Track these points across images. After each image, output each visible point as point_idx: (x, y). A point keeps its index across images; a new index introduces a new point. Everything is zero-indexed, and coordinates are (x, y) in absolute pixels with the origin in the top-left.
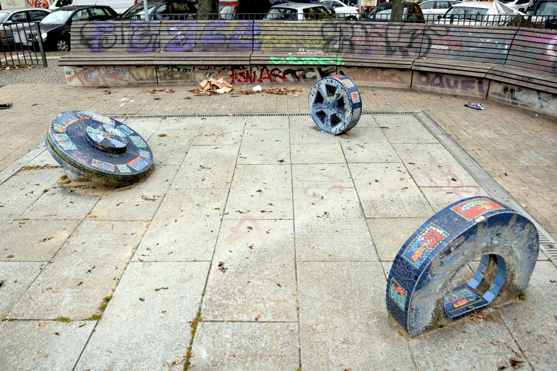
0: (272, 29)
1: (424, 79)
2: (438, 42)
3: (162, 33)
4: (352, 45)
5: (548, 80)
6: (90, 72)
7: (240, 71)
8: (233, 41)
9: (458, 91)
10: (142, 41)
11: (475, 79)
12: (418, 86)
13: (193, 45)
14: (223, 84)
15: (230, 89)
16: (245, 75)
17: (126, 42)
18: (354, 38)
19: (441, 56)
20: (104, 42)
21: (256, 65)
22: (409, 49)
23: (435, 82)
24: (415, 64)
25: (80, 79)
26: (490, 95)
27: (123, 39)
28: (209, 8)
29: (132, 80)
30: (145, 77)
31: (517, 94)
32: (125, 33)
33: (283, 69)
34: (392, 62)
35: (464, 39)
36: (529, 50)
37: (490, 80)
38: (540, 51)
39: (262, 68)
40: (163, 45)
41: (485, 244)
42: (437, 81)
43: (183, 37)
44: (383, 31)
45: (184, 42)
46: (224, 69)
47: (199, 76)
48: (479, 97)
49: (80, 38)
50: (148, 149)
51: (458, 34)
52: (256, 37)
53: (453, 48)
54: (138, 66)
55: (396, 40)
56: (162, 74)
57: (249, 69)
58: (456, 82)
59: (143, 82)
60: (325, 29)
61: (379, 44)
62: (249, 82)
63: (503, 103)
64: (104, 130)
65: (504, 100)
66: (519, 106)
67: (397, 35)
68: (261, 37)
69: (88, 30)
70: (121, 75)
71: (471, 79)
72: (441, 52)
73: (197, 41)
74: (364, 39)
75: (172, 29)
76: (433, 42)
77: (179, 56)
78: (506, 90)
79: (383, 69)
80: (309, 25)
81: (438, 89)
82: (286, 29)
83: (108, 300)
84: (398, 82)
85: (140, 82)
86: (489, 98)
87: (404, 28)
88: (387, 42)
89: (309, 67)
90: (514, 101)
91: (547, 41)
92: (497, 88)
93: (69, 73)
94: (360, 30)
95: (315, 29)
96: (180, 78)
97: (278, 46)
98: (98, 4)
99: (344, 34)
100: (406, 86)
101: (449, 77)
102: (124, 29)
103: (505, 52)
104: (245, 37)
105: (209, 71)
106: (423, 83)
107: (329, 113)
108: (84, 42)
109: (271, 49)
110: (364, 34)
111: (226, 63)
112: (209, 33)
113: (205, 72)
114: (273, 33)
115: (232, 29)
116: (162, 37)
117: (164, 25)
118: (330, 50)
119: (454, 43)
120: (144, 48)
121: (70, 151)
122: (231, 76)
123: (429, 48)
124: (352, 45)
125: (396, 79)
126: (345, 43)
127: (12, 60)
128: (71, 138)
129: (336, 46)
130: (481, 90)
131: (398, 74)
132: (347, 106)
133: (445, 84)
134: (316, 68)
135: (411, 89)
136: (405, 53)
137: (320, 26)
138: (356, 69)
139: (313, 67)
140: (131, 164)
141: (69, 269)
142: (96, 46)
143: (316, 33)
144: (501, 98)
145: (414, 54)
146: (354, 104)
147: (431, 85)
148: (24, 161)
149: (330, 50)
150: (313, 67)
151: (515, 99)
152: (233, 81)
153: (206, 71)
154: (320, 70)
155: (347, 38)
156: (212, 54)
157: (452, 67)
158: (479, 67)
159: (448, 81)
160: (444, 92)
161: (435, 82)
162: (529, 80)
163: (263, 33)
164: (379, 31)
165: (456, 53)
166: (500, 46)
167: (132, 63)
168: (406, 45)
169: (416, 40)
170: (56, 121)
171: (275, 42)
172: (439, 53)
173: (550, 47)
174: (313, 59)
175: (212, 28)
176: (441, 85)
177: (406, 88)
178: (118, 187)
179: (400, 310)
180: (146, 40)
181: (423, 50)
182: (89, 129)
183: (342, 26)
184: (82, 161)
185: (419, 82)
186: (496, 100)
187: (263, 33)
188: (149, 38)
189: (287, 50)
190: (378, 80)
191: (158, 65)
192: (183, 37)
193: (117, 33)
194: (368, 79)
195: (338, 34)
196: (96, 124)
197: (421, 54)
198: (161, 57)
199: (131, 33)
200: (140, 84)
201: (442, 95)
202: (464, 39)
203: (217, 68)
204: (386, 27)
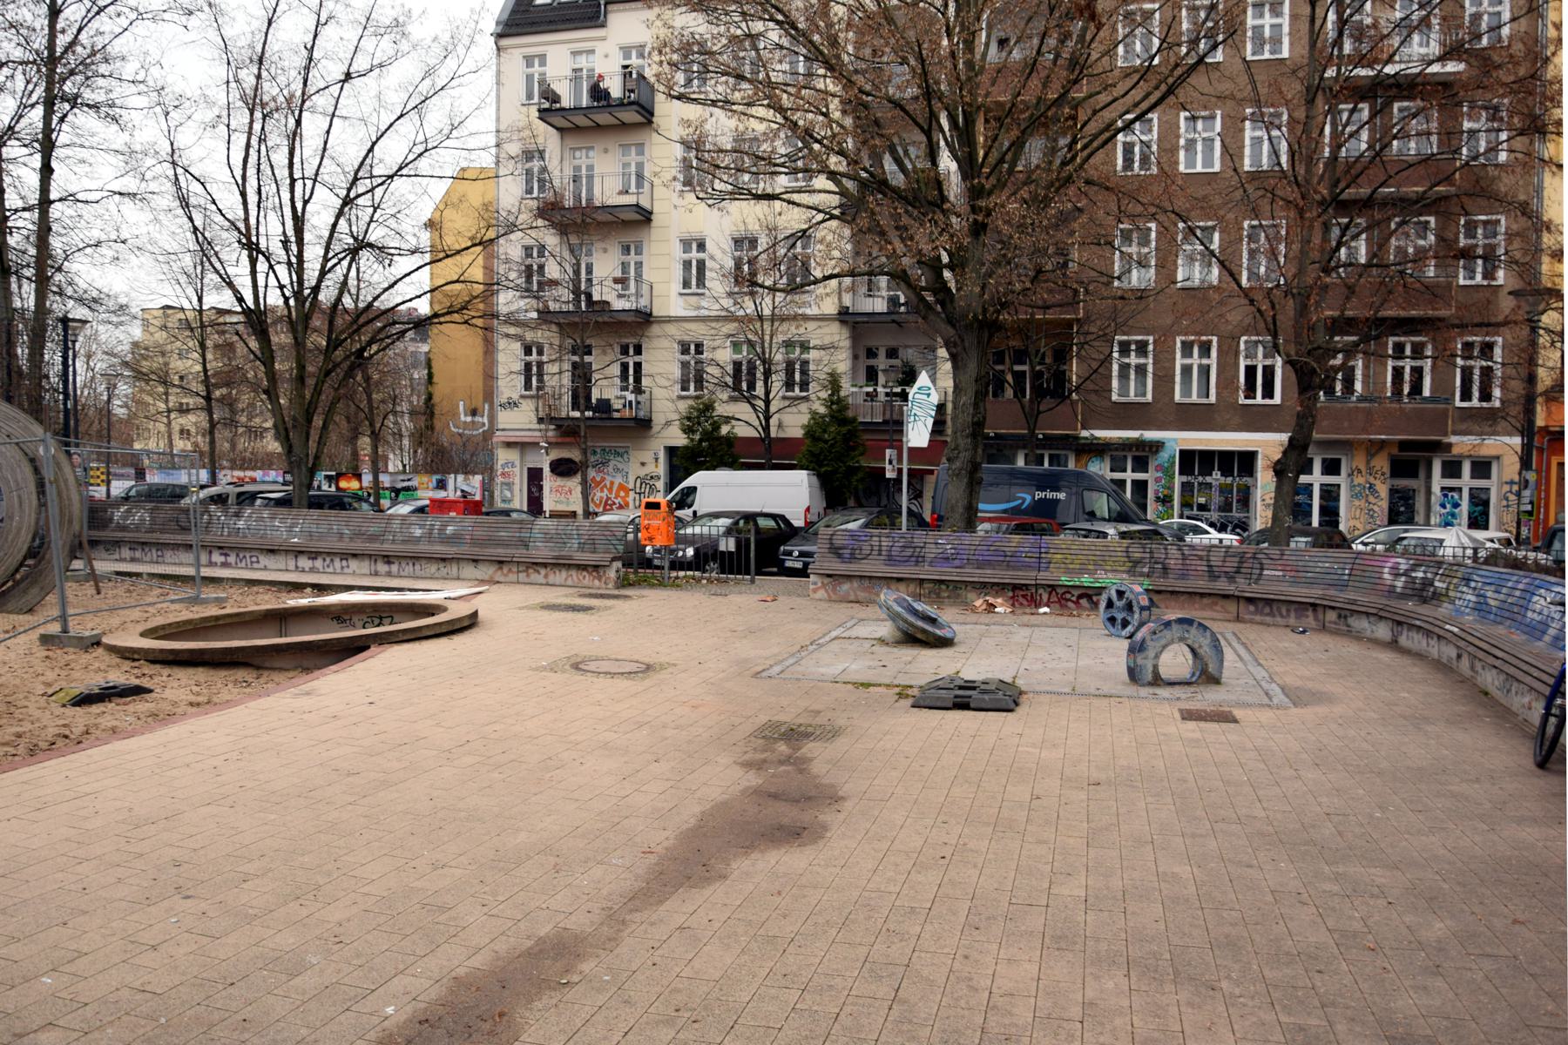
1: (1252, 608)
9: (1292, 621)
21: (1043, 586)
31: (1351, 621)
33: (1076, 593)
37: (1325, 606)
42: (1267, 610)
47: (971, 596)
77: (949, 573)
78: (1340, 616)
81: (1268, 619)
92: (1331, 616)
98: (766, 510)
107: (1119, 616)
129: (1146, 570)
130: (1316, 619)
131: (1222, 602)
132: (1136, 609)
135: (1238, 619)
136: (1231, 579)
162: (1354, 602)
172: (1272, 579)
176: (1271, 614)
180: (909, 552)
185: (1247, 611)
189: (1082, 571)
198: (926, 572)
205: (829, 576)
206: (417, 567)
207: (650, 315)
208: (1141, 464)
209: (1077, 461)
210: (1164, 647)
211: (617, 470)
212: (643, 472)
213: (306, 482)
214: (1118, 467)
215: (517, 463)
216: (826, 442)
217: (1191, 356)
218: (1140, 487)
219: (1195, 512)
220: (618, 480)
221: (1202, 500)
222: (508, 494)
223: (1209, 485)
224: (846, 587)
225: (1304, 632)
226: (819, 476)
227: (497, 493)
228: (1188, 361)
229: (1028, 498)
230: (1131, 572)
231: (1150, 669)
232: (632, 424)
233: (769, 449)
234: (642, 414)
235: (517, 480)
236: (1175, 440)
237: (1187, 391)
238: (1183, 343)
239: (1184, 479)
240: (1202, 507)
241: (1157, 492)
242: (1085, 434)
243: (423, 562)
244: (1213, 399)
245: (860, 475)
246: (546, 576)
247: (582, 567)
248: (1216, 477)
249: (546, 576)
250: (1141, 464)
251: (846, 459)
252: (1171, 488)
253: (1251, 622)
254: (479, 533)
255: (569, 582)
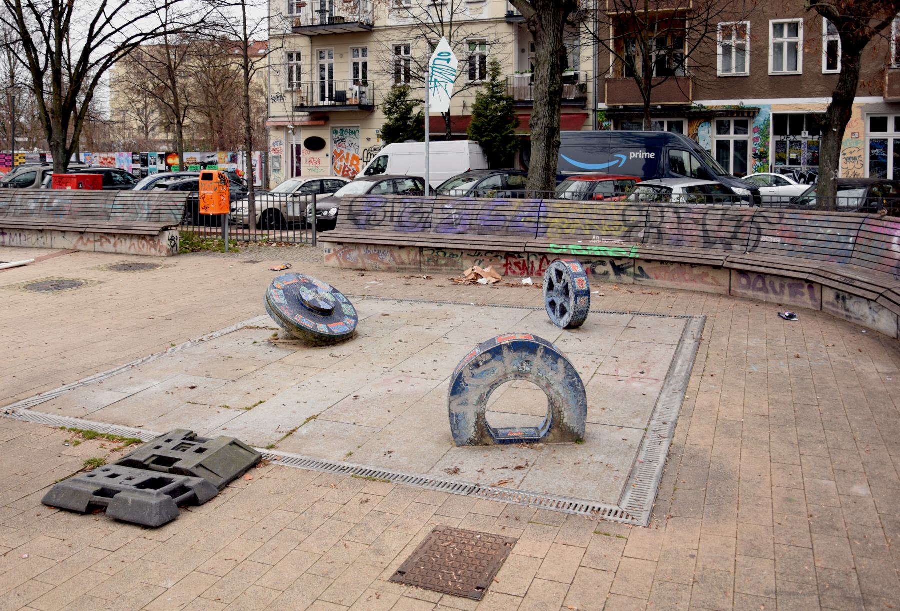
0: (562, 210)
1: (744, 281)
2: (770, 232)
3: (435, 211)
4: (660, 233)
5: (873, 282)
6: (350, 251)
7: (515, 260)
8: (514, 224)
10: (413, 220)
11: (804, 282)
12: (739, 291)
13: (468, 227)
14: (488, 273)
15: (495, 280)
16: (521, 266)
17: (395, 219)
18: (663, 225)
19: (773, 251)
20: (372, 218)
21: (534, 253)
22: (733, 241)
23: (758, 286)
24: (729, 259)
25: (338, 258)
26: (824, 305)
27: (392, 216)
28: (541, 184)
29: (393, 264)
30: (407, 261)
31: (850, 303)
32: (396, 209)
34: (700, 256)
35: (800, 229)
36: (874, 244)
38: (885, 246)
39: (541, 257)
40: (434, 225)
41: (515, 367)
42: (760, 284)
43: (457, 216)
44: (701, 216)
45: (458, 222)
46: (497, 256)
47: (467, 263)
48: (811, 307)
49: (348, 212)
50: (355, 318)
51: (793, 222)
52: (542, 220)
53: (787, 240)
54: (401, 247)
55: (716, 228)
56: (426, 258)
57: (526, 258)
58: (782, 286)
59: (404, 266)
60: (627, 213)
61: (694, 233)
62: (526, 275)
63: (838, 317)
64: (317, 292)
65: (838, 313)
66: (853, 320)
67: (718, 223)
68: (547, 220)
69: (358, 204)
70: (382, 256)
71: (799, 282)
72: (772, 246)
73: (473, 222)
74: (676, 226)
75: (446, 206)
76: (764, 232)
77: (448, 238)
78: (838, 297)
79: (692, 265)
80: (608, 207)
81: (761, 295)
82: (579, 211)
83: (261, 402)
84: (712, 284)
85: (401, 266)
86: (824, 310)
87: (728, 213)
88: (705, 231)
89: (599, 259)
90: (848, 313)
91: (892, 232)
93: (328, 251)
94: (671, 215)
95: (615, 212)
96: (446, 265)
97: (567, 231)
99: (652, 219)
100: (723, 290)
101: (773, 278)
102: (396, 205)
103: (850, 247)
104: (528, 219)
105: (478, 258)
106: (744, 287)
107: (559, 301)
108: (351, 217)
109: (559, 235)
110: (676, 220)
111: (497, 248)
112: (487, 212)
113: (474, 259)
114: (563, 215)
115: (515, 209)
116: (434, 216)
117: (439, 202)
118: (632, 239)
119: (787, 234)
120: (413, 227)
121: (281, 304)
122: (506, 265)
123: (758, 241)
124: (660, 233)
125: (709, 280)
126: (651, 231)
127: (281, 237)
128: (286, 295)
129: (641, 235)
130: (812, 297)
131: (712, 273)
132: (572, 294)
133: (770, 288)
134: (607, 261)
135: (730, 294)
136: (727, 245)
137: (622, 208)
138: (658, 264)
139: (604, 259)
140: (331, 326)
141: (244, 386)
142: (363, 222)
143: (616, 217)
144: (835, 309)
145: (739, 247)
146: (586, 295)
147: (753, 289)
148: (248, 323)
149: (632, 239)
150: (604, 259)
151: (847, 310)
152: (507, 272)
153: (476, 258)
154: (613, 264)
155: (654, 224)
156: (488, 238)
157: (771, 265)
158: (807, 265)
159: (772, 284)
160: (769, 300)
161: (758, 286)
163: (550, 215)
164: (696, 216)
165: (790, 248)
166: (843, 239)
167: (394, 243)
168: (730, 235)
169: (742, 230)
170: (278, 279)
171: (565, 226)
173: (895, 240)
174: (601, 248)
175: (491, 208)
176: (764, 289)
177: (724, 292)
178: (315, 346)
179: (39, 68)
181: (752, 243)
182: (303, 288)
183: (651, 208)
184: (288, 314)
185: (740, 285)
186: (831, 313)
187: (550, 215)
188: (420, 215)
189: (576, 237)
190: (687, 281)
191: (422, 247)
192: (457, 216)
193: (387, 209)
194: (673, 279)
195: (644, 219)
196: (310, 285)
197: (749, 248)
199: (402, 210)
200: (400, 269)
201: (757, 302)
202: (800, 229)
203: (489, 255)
204: (705, 211)
205: (340, 243)
206: (23, 238)
207: (372, 26)
208: (742, 127)
209: (690, 126)
210: (493, 386)
211: (352, 145)
212: (369, 145)
213: (62, 161)
214: (722, 128)
215: (284, 141)
216: (487, 117)
217: (782, 36)
218: (741, 147)
219: (788, 166)
220: (353, 152)
221: (793, 156)
222: (277, 165)
223: (799, 143)
224: (355, 254)
225: (791, 316)
226: (481, 144)
227: (270, 164)
228: (779, 40)
229: (624, 158)
230: (626, 237)
231: (473, 420)
232: (357, 109)
233: (449, 126)
234: (365, 102)
235: (284, 155)
236: (769, 106)
237: (778, 65)
238: (775, 25)
239: (778, 138)
240: (794, 162)
241: (755, 150)
242: (697, 103)
243: (27, 233)
244: (800, 70)
245: (513, 143)
246: (115, 245)
247: (142, 237)
248: (805, 136)
249: (115, 245)
250: (742, 127)
251: (499, 133)
252: (766, 146)
253: (743, 298)
254: (77, 206)
255: (133, 251)
